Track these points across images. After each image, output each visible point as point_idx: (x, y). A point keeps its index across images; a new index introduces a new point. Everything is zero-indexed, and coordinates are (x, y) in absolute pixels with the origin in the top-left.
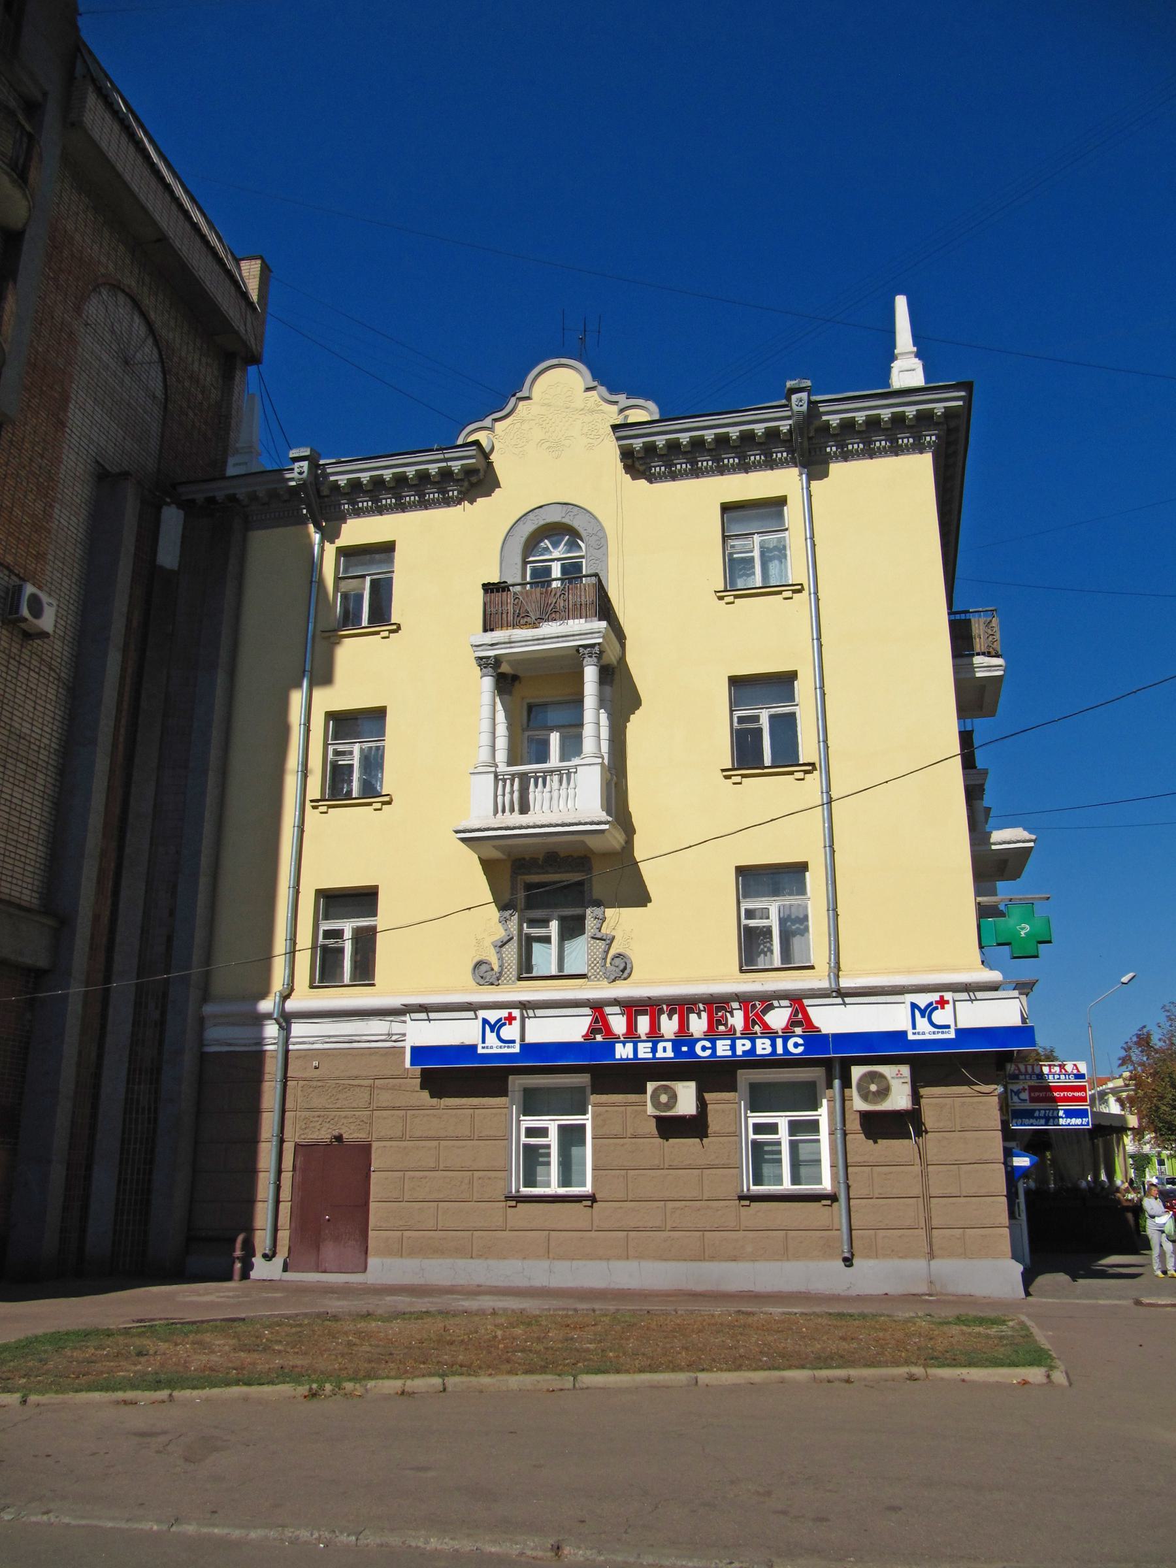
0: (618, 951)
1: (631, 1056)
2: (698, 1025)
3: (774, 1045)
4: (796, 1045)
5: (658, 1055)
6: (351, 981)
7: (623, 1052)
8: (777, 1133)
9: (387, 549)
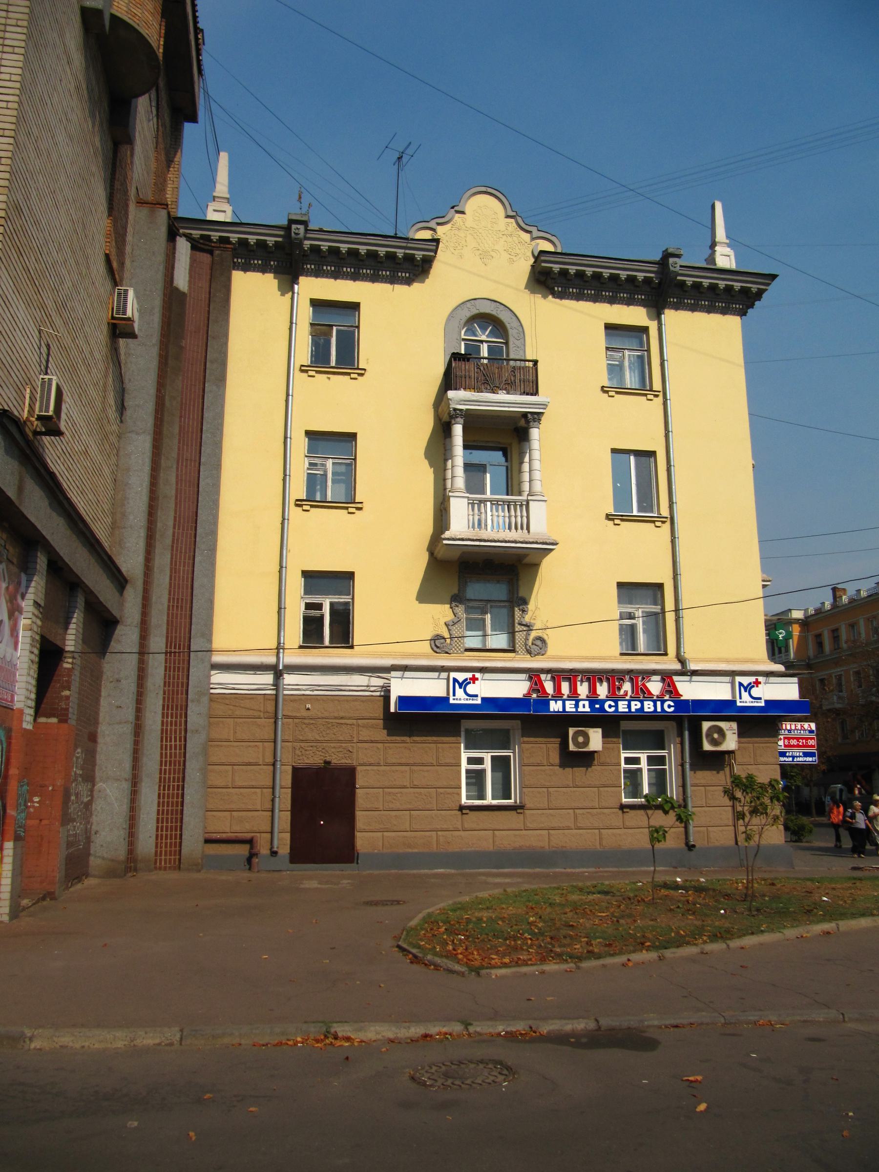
0: (545, 637)
1: (561, 710)
2: (602, 690)
3: (655, 706)
4: (669, 706)
5: (579, 710)
6: (648, 650)
7: (555, 706)
8: (640, 764)
9: (355, 307)
